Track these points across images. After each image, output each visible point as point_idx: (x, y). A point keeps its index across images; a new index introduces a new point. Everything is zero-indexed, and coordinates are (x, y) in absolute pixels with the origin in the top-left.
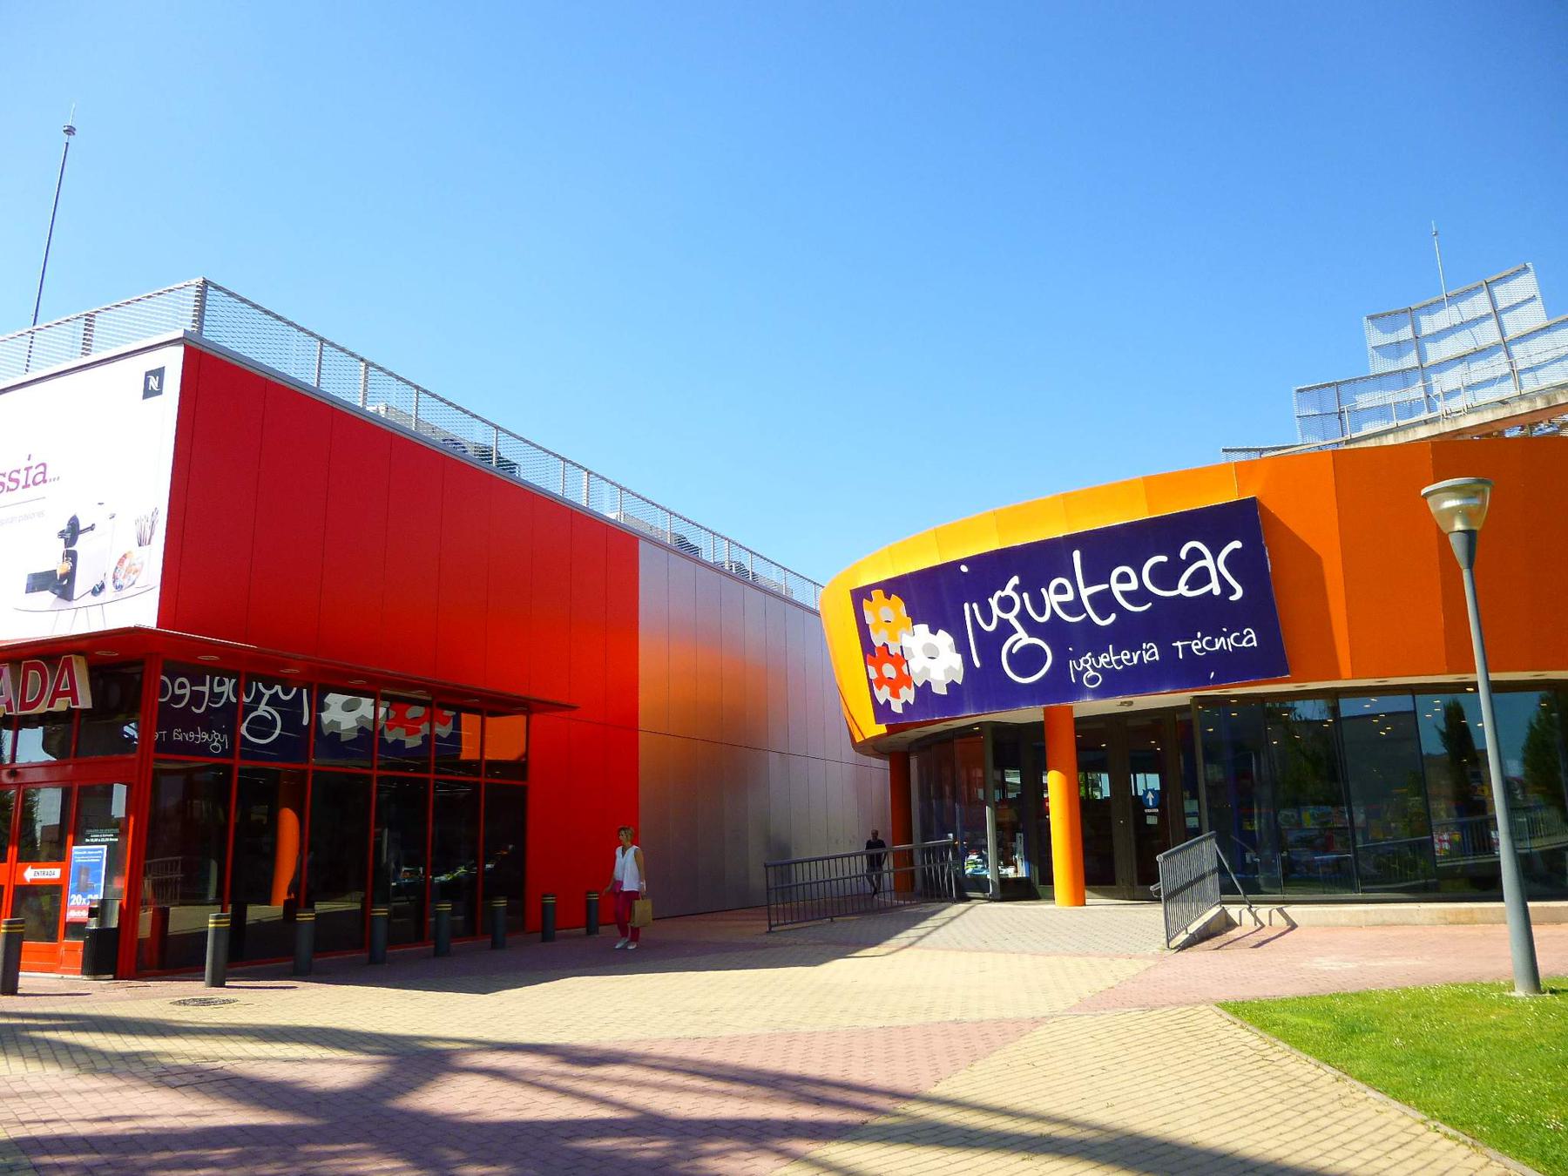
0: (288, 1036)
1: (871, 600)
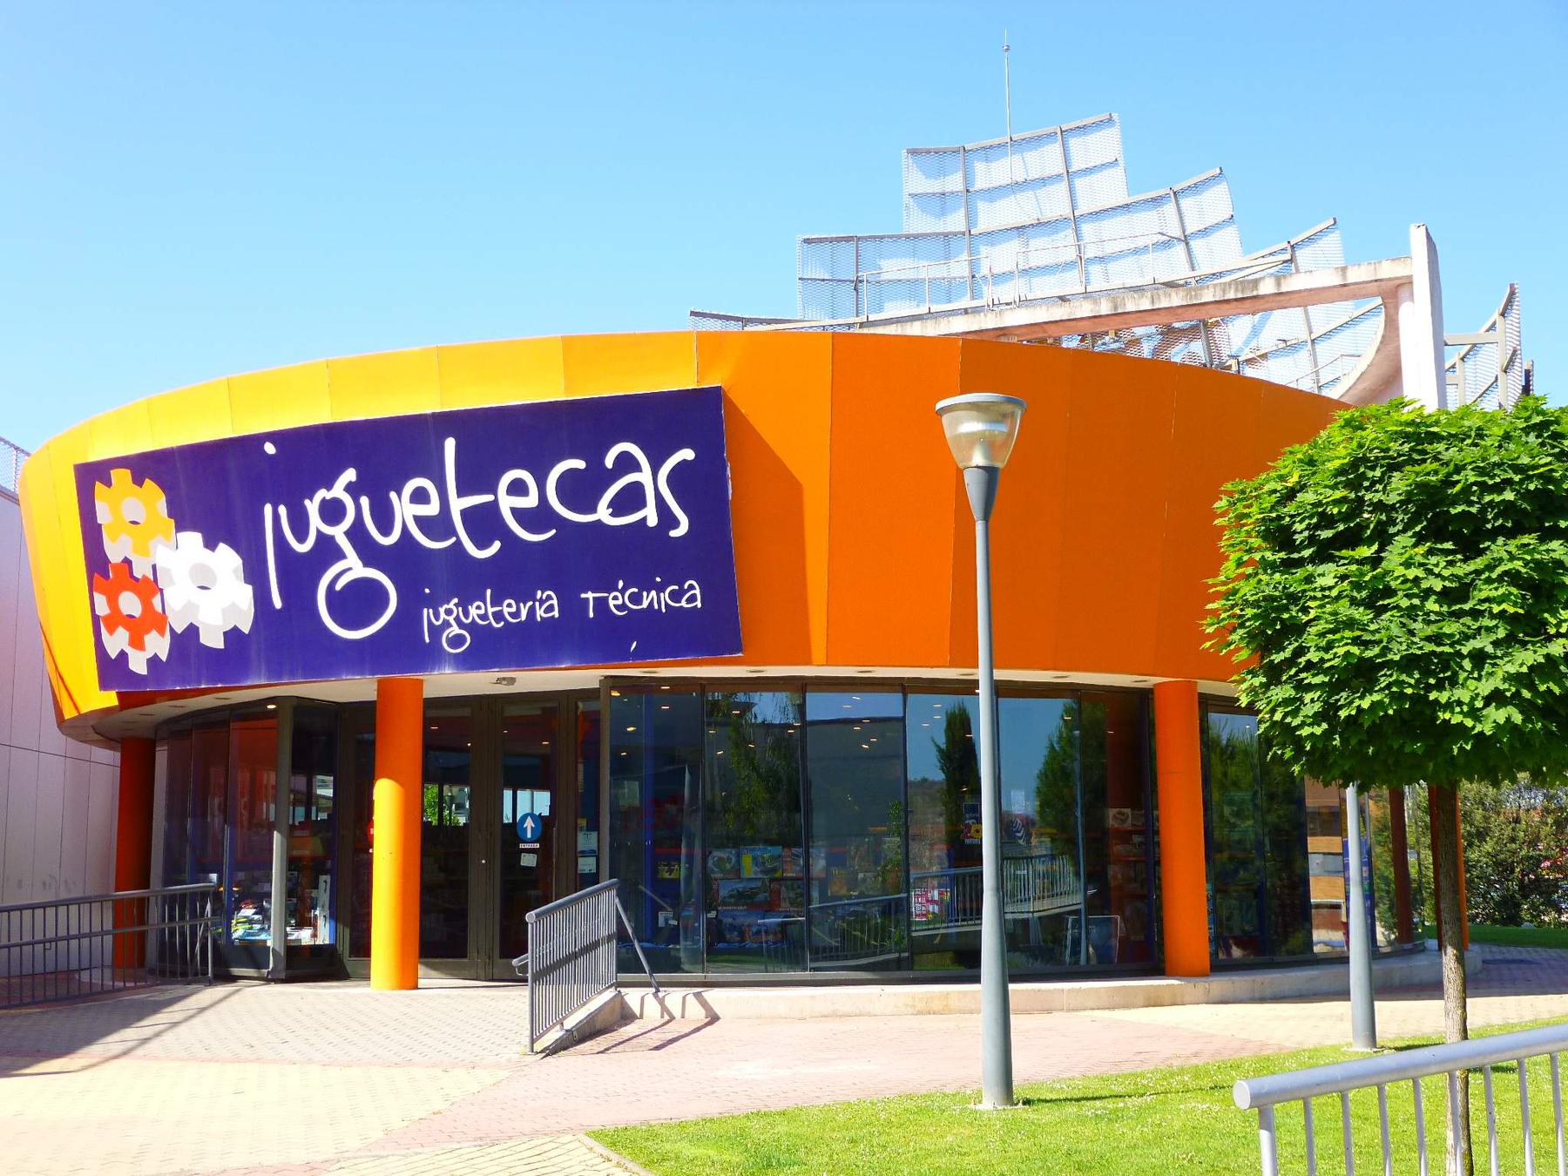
1: (108, 483)
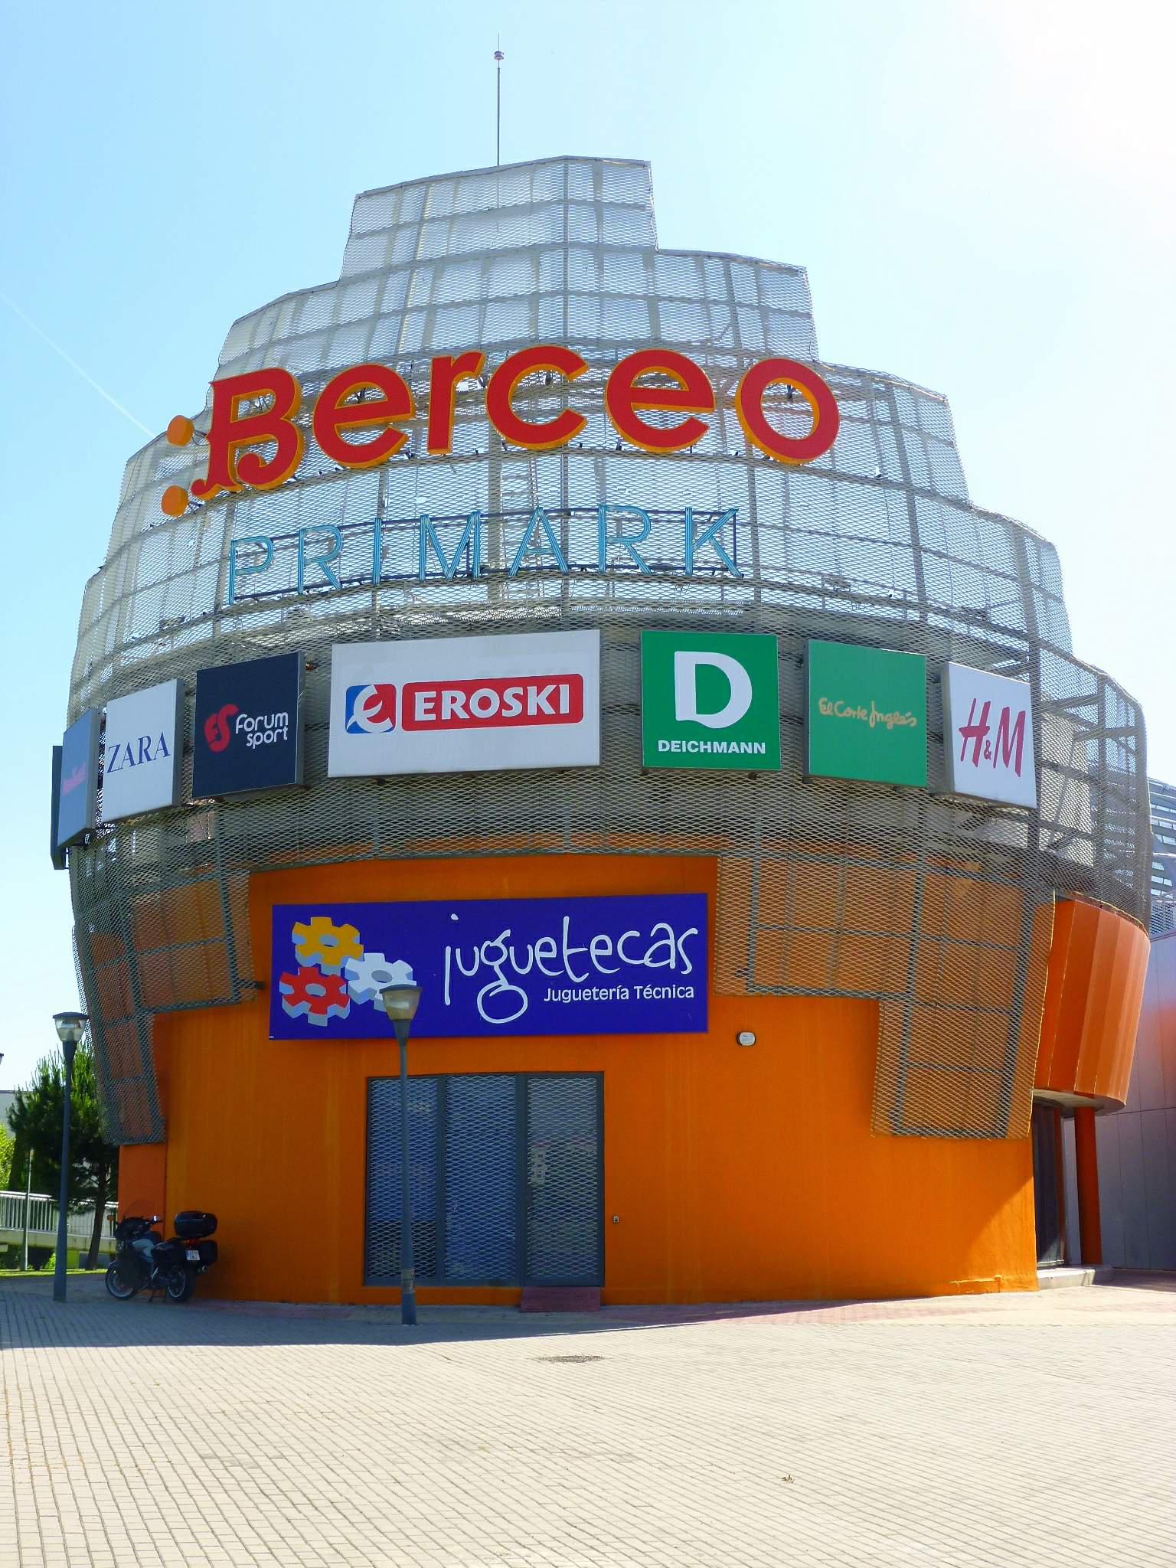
0: (120, 552)
